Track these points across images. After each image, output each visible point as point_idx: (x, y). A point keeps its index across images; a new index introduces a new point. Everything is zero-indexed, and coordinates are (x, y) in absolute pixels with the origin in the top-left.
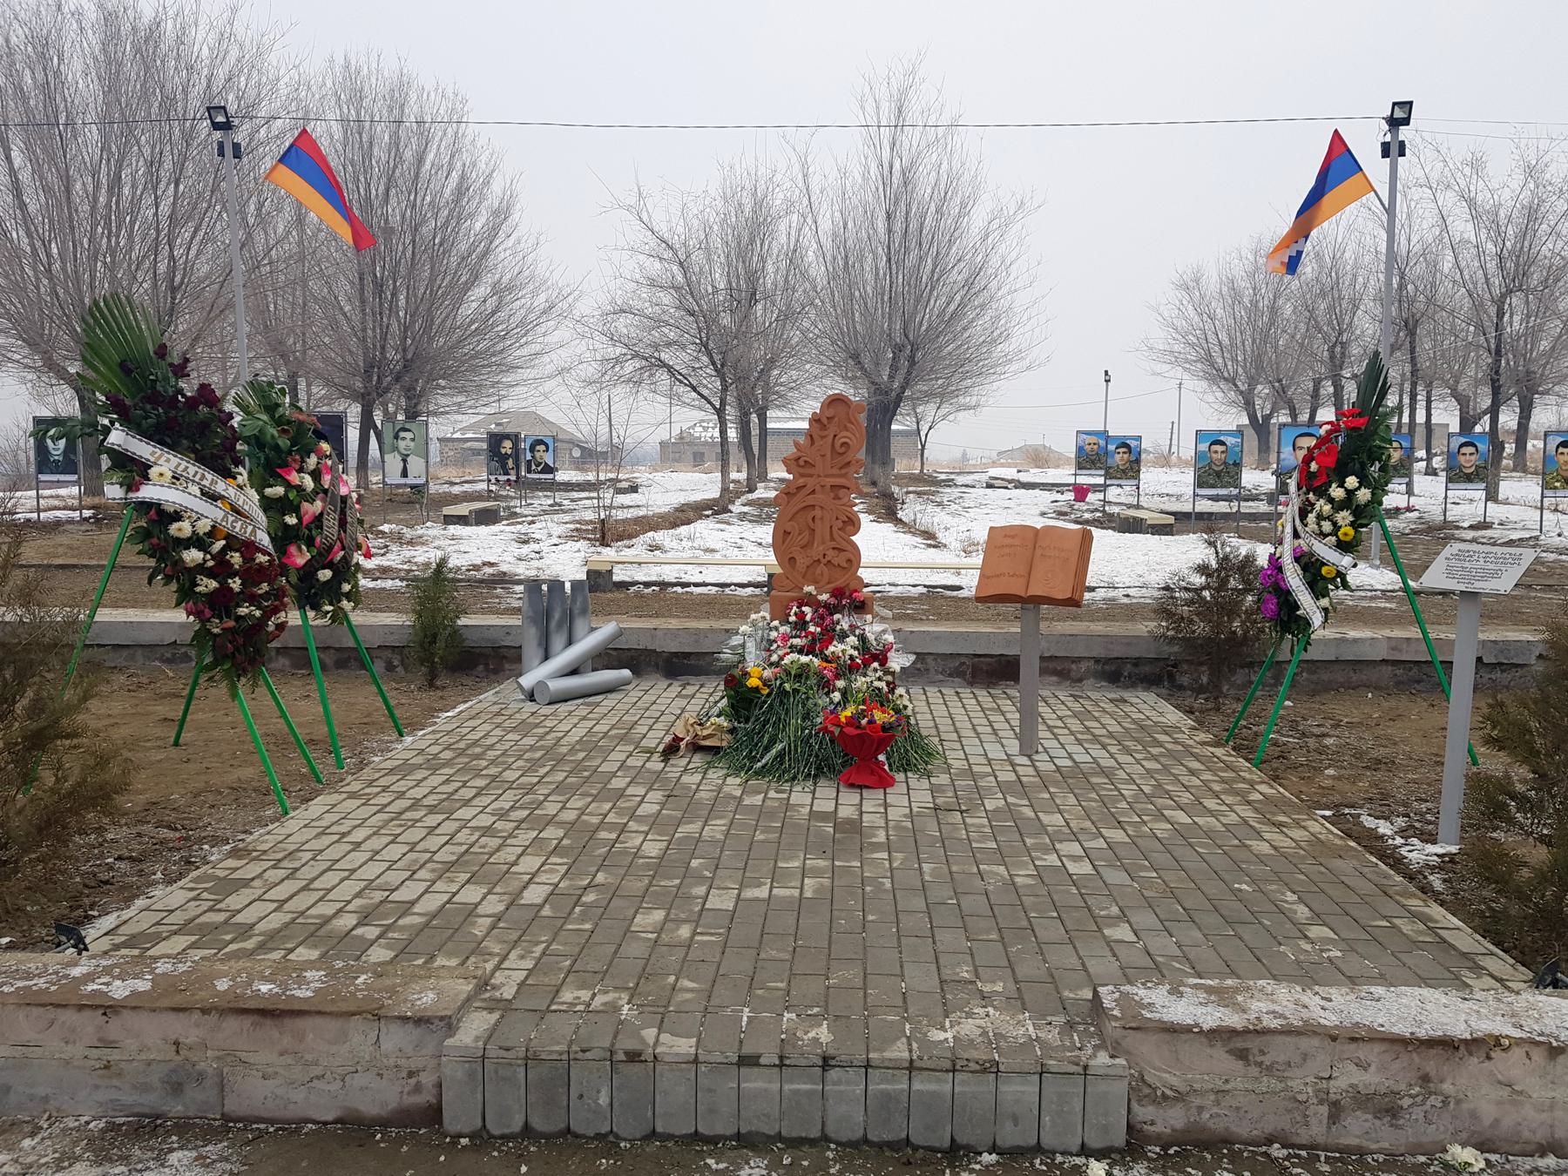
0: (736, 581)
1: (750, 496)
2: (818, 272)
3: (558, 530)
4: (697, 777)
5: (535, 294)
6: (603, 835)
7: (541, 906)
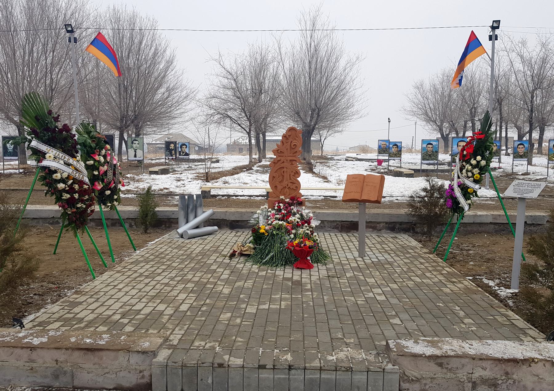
1: (260, 164)
2: (284, 83)
3: (191, 176)
4: (242, 265)
5: (182, 91)
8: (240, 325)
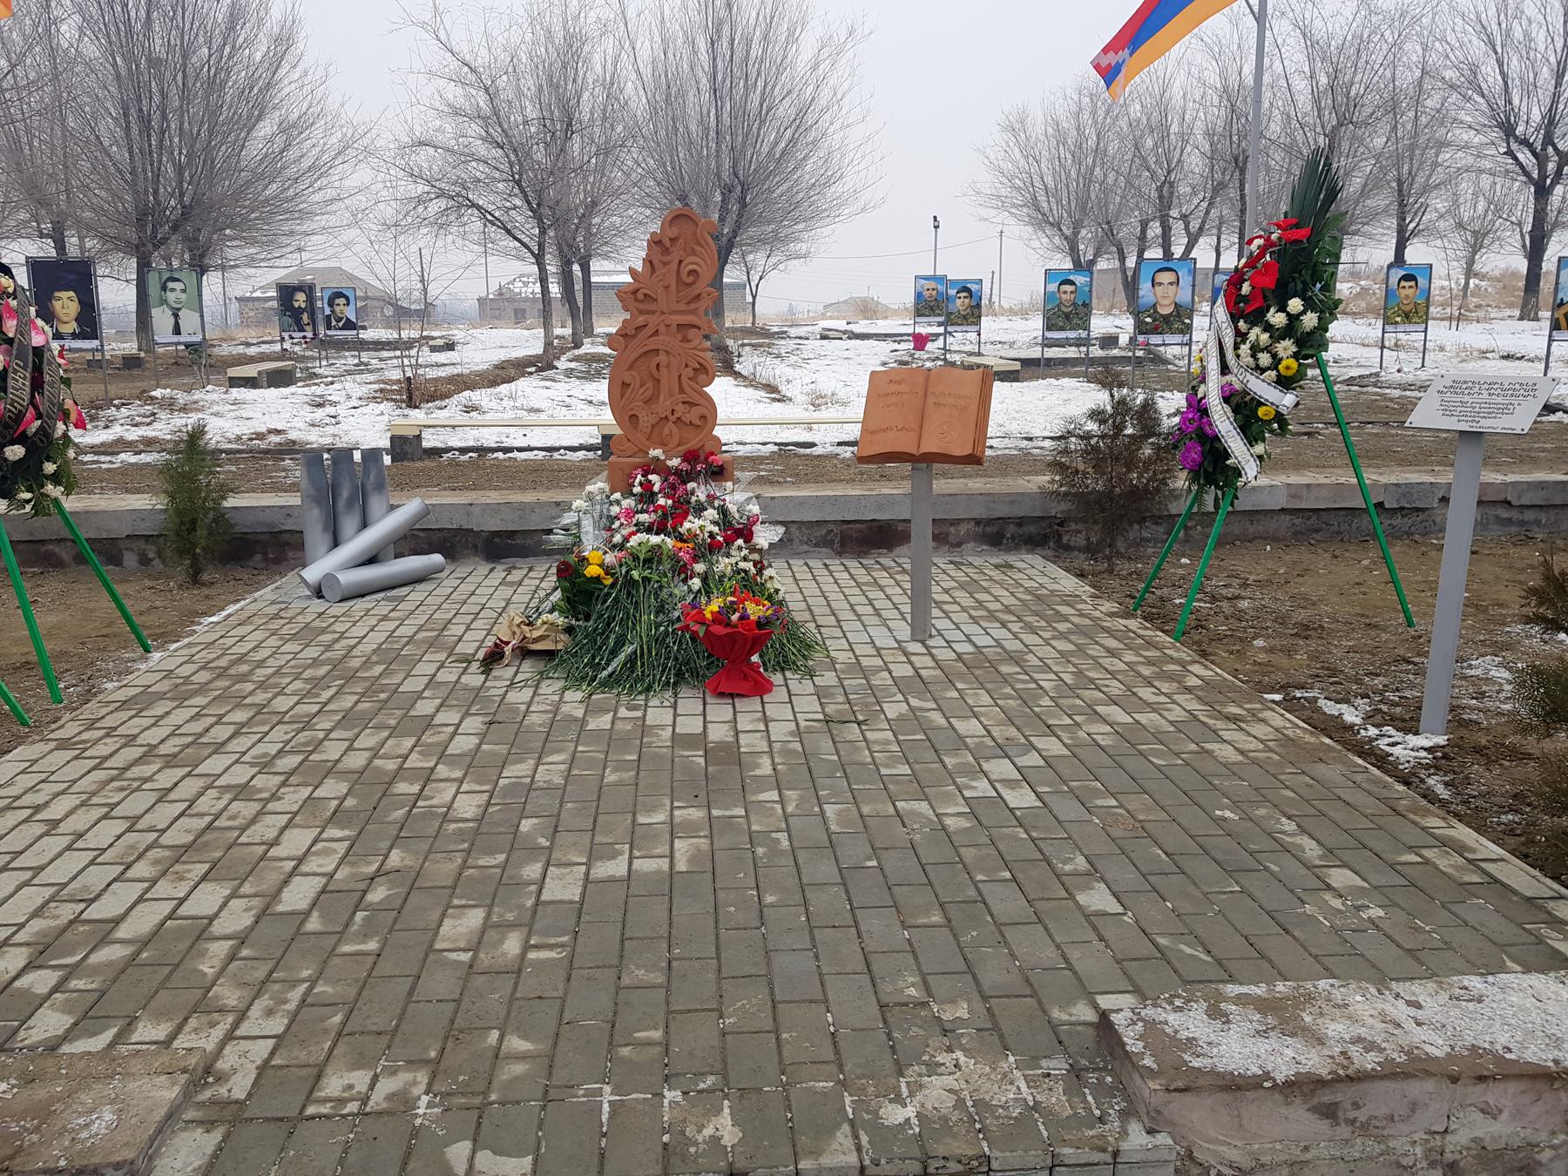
0: (565, 444)
1: (576, 352)
3: (364, 390)
4: (527, 694)
5: (327, 132)
6: (402, 787)
7: (306, 914)
8: (517, 970)
